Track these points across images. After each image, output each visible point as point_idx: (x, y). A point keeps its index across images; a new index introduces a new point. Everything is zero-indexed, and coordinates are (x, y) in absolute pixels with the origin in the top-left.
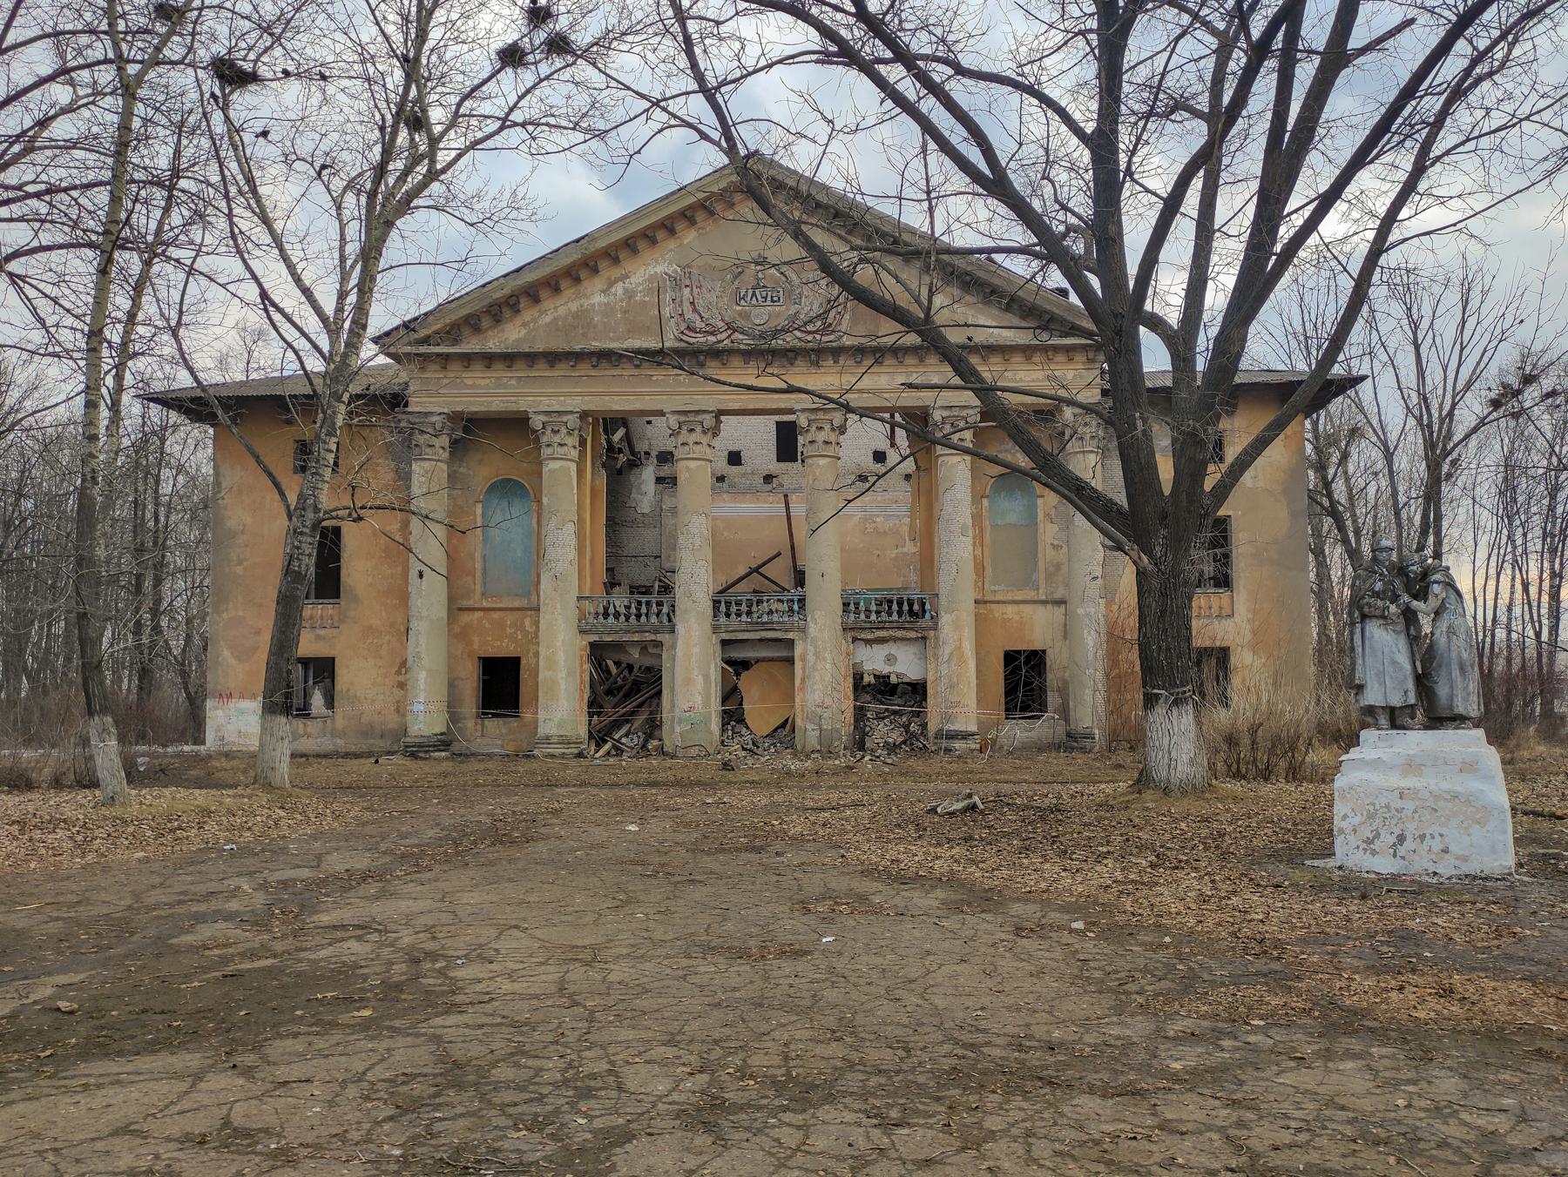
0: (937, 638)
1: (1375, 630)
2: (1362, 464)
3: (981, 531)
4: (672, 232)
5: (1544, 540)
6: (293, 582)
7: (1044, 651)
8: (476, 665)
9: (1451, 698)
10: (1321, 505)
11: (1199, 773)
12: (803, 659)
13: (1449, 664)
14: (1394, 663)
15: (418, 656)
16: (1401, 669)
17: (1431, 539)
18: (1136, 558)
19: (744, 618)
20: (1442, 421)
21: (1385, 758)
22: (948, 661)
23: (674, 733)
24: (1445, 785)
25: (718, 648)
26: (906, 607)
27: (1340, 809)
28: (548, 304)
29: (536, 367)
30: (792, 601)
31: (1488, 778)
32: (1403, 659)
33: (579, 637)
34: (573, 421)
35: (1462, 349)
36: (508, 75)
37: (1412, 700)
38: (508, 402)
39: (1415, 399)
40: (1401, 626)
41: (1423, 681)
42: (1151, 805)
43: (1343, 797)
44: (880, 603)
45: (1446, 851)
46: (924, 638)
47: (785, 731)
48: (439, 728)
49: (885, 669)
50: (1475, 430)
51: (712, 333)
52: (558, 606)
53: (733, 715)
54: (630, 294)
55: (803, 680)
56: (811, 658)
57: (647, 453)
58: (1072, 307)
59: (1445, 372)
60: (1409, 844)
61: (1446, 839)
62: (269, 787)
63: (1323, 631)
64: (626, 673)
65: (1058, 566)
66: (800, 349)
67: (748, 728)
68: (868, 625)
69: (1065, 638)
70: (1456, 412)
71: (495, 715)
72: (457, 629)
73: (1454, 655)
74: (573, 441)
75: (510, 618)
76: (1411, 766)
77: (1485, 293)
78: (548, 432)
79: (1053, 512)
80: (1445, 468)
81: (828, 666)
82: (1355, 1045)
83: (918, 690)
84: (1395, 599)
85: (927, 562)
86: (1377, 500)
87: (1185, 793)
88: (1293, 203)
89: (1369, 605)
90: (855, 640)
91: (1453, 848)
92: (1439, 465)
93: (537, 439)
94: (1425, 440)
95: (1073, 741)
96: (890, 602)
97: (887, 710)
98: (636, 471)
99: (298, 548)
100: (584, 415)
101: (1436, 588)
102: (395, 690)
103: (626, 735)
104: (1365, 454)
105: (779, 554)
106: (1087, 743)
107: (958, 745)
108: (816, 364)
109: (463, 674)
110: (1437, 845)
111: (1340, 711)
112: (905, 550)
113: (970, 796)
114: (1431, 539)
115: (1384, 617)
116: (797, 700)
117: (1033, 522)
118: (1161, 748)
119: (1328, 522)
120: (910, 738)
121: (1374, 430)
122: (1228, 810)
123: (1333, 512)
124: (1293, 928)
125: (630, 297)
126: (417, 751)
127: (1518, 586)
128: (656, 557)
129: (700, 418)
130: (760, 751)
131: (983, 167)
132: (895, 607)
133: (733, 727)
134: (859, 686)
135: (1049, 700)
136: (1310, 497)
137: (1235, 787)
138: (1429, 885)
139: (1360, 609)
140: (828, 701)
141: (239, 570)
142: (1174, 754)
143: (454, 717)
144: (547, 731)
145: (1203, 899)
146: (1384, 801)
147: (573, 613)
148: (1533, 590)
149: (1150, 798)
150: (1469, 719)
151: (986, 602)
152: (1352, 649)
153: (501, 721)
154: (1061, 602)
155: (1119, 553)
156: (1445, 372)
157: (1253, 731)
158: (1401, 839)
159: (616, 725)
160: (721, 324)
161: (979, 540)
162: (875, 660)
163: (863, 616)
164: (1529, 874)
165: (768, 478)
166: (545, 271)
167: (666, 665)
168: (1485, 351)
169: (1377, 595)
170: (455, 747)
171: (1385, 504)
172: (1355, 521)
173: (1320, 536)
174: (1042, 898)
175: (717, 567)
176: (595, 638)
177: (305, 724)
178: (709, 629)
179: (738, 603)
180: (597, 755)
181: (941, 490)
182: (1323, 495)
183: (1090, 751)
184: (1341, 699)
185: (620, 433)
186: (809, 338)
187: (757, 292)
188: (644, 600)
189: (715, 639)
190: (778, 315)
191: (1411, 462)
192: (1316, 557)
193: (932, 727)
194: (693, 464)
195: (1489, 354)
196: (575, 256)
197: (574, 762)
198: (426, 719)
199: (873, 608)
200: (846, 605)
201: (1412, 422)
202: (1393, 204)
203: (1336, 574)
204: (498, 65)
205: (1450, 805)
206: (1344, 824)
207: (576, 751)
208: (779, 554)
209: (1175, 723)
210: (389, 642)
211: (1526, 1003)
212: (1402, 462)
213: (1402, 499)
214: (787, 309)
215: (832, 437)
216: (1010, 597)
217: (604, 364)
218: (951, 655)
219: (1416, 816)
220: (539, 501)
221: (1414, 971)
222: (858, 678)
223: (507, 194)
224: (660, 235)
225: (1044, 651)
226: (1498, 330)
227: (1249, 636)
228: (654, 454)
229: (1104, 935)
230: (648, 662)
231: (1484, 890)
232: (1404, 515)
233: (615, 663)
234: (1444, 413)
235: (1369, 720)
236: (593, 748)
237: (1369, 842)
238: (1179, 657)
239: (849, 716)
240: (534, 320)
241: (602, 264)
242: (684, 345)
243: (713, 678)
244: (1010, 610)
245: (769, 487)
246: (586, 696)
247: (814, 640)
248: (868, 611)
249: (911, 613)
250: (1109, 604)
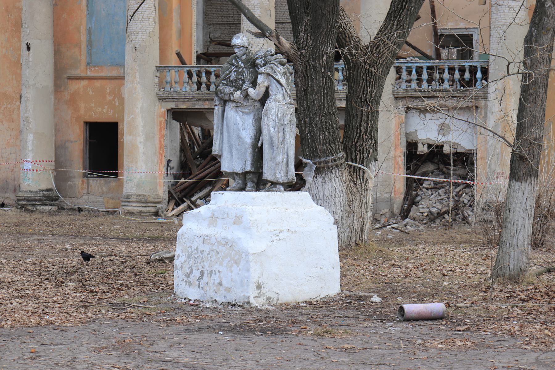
0: (486, 106)
15: (27, 120)
26: (457, 75)
33: (157, 103)
52: (137, 75)
61: (221, 275)
68: (419, 94)
91: (224, 282)
144: (129, 191)
176: (172, 105)
179: (442, 72)
188: (212, 70)
207: (153, 210)
209: (320, 188)
219: (209, 256)
222: (412, 146)
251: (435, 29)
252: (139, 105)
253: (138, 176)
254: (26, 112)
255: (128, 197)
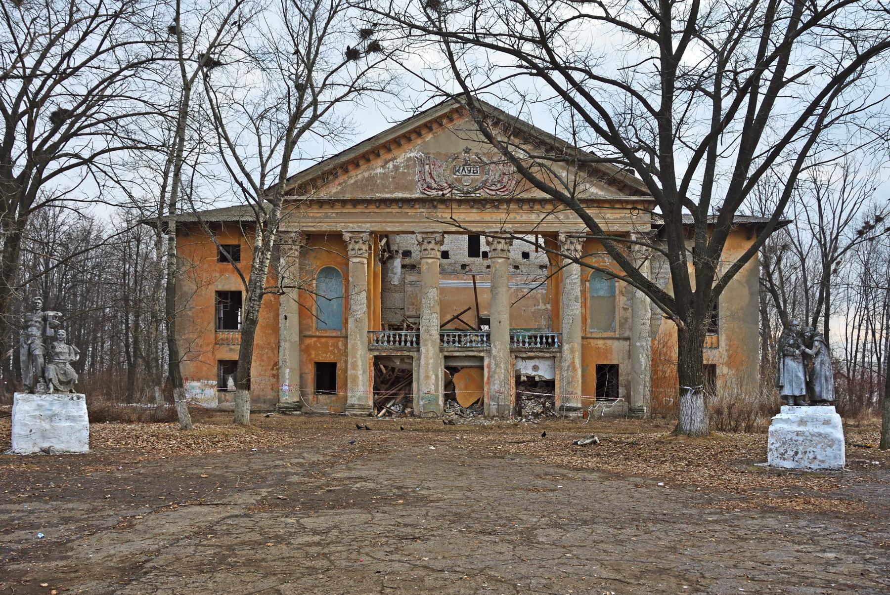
0: (561, 357)
1: (789, 362)
2: (788, 264)
3: (585, 299)
4: (419, 135)
5: (884, 308)
6: (250, 324)
7: (618, 365)
8: (313, 366)
9: (821, 392)
10: (765, 286)
11: (704, 427)
12: (489, 367)
13: (820, 377)
14: (797, 376)
15: (285, 360)
16: (800, 379)
17: (824, 306)
18: (678, 323)
19: (457, 344)
20: (831, 243)
21: (791, 418)
22: (567, 370)
23: (418, 405)
24: (816, 430)
25: (443, 361)
26: (544, 340)
27: (771, 440)
28: (352, 173)
29: (346, 207)
30: (483, 336)
31: (835, 427)
32: (801, 375)
34: (365, 236)
35: (843, 203)
36: (351, 63)
37: (804, 393)
38: (331, 226)
39: (817, 229)
40: (801, 360)
41: (809, 385)
42: (682, 441)
43: (772, 435)
44: (530, 338)
45: (815, 458)
46: (554, 357)
47: (478, 406)
48: (296, 399)
49: (532, 373)
50: (848, 248)
51: (441, 190)
52: (358, 336)
53: (450, 397)
54: (396, 168)
55: (488, 378)
56: (493, 366)
57: (397, 251)
58: (637, 179)
59: (834, 214)
60: (800, 455)
62: (242, 424)
63: (765, 356)
64: (391, 373)
65: (626, 320)
66: (489, 199)
67: (458, 403)
68: (523, 349)
69: (629, 358)
70: (839, 237)
71: (323, 393)
72: (303, 347)
73: (823, 373)
74: (365, 247)
75: (331, 342)
76: (802, 422)
77: (856, 172)
78: (353, 242)
79: (624, 290)
80: (833, 267)
81: (503, 371)
82: (773, 515)
83: (550, 385)
84: (798, 347)
85: (555, 316)
86: (796, 284)
87: (698, 436)
88: (757, 152)
89: (787, 350)
90: (516, 357)
91: (819, 457)
92: (829, 267)
93: (346, 247)
94: (822, 252)
95: (632, 413)
96: (536, 337)
97: (533, 395)
98: (391, 261)
99: (252, 307)
100: (371, 233)
101: (816, 343)
102: (271, 379)
103: (393, 405)
104: (790, 258)
105: (469, 309)
106: (640, 414)
107: (572, 414)
108: (497, 207)
109: (307, 371)
110: (811, 456)
111: (772, 399)
112: (539, 307)
113: (593, 437)
114: (824, 306)
115: (793, 356)
116: (485, 389)
117: (613, 296)
118: (687, 415)
119: (769, 295)
120: (546, 410)
121: (796, 246)
122: (718, 444)
123: (772, 291)
124: (750, 485)
125: (397, 170)
126: (286, 410)
127: (870, 332)
128: (401, 309)
129: (434, 236)
130: (465, 415)
131: (605, 128)
132: (538, 340)
133: (450, 403)
134: (518, 383)
135: (620, 391)
136: (760, 282)
137: (722, 434)
138: (807, 472)
139: (783, 352)
140: (502, 390)
141: (190, 313)
142: (693, 418)
143: (303, 394)
145: (711, 476)
146: (789, 437)
147: (366, 340)
148: (877, 336)
149: (681, 438)
150: (829, 401)
151: (587, 338)
152: (779, 370)
153: (327, 396)
154: (627, 339)
155: (671, 321)
156: (834, 214)
157: (730, 407)
158: (796, 453)
159: (388, 400)
160: (445, 185)
161: (584, 305)
162: (527, 369)
163: (521, 345)
164: (850, 468)
165: (464, 266)
166: (352, 155)
167: (415, 369)
168: (855, 204)
169: (790, 346)
170: (303, 409)
171: (800, 286)
172: (784, 296)
173: (765, 303)
174: (644, 476)
175: (442, 314)
176: (377, 353)
177: (225, 395)
178: (438, 350)
180: (379, 415)
181: (564, 278)
182: (766, 280)
183: (641, 419)
184: (773, 393)
185: (384, 241)
186: (494, 193)
187: (465, 168)
189: (441, 355)
190: (477, 180)
191: (814, 261)
192: (762, 314)
193: (558, 404)
194: (430, 261)
195: (857, 206)
196: (368, 148)
197: (367, 419)
198: (289, 395)
199: (527, 340)
200: (512, 338)
201: (815, 242)
202: (805, 147)
203: (772, 323)
204: (346, 59)
205: (818, 439)
206: (772, 447)
207: (368, 413)
208: (469, 309)
210: (267, 353)
211: (836, 505)
212: (809, 263)
213: (809, 284)
214: (482, 177)
215: (506, 247)
216: (600, 335)
217: (382, 206)
218: (568, 367)
220: (347, 280)
221: (796, 497)
222: (518, 377)
223: (341, 120)
224: (413, 136)
225: (618, 365)
226: (863, 193)
227: (726, 359)
228: (401, 252)
229: (674, 487)
230: (404, 366)
231: (830, 474)
232: (810, 292)
233: (384, 367)
234: (833, 237)
235: (785, 401)
236: (376, 412)
237: (783, 454)
238: (697, 371)
239: (513, 398)
240: (345, 182)
241: (382, 152)
242: (425, 196)
243: (440, 376)
244: (600, 342)
245: (464, 271)
246: (372, 384)
247: (495, 357)
248: (518, 342)
249: (547, 343)
250: (653, 339)
251: (478, 315)
252: (359, 353)
253: (359, 394)
254: (284, 355)
255: (353, 405)
